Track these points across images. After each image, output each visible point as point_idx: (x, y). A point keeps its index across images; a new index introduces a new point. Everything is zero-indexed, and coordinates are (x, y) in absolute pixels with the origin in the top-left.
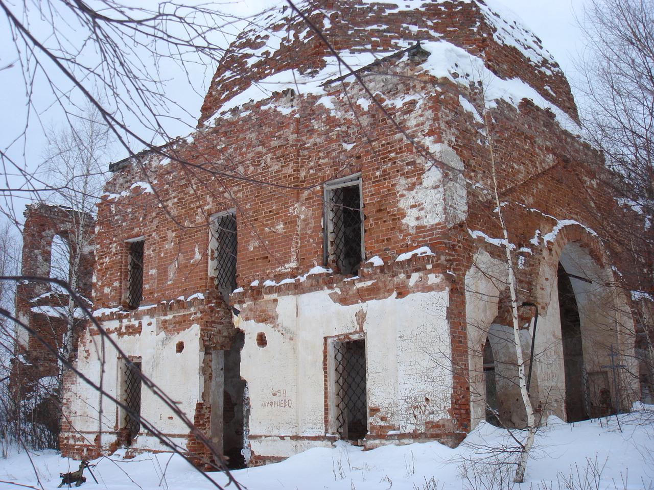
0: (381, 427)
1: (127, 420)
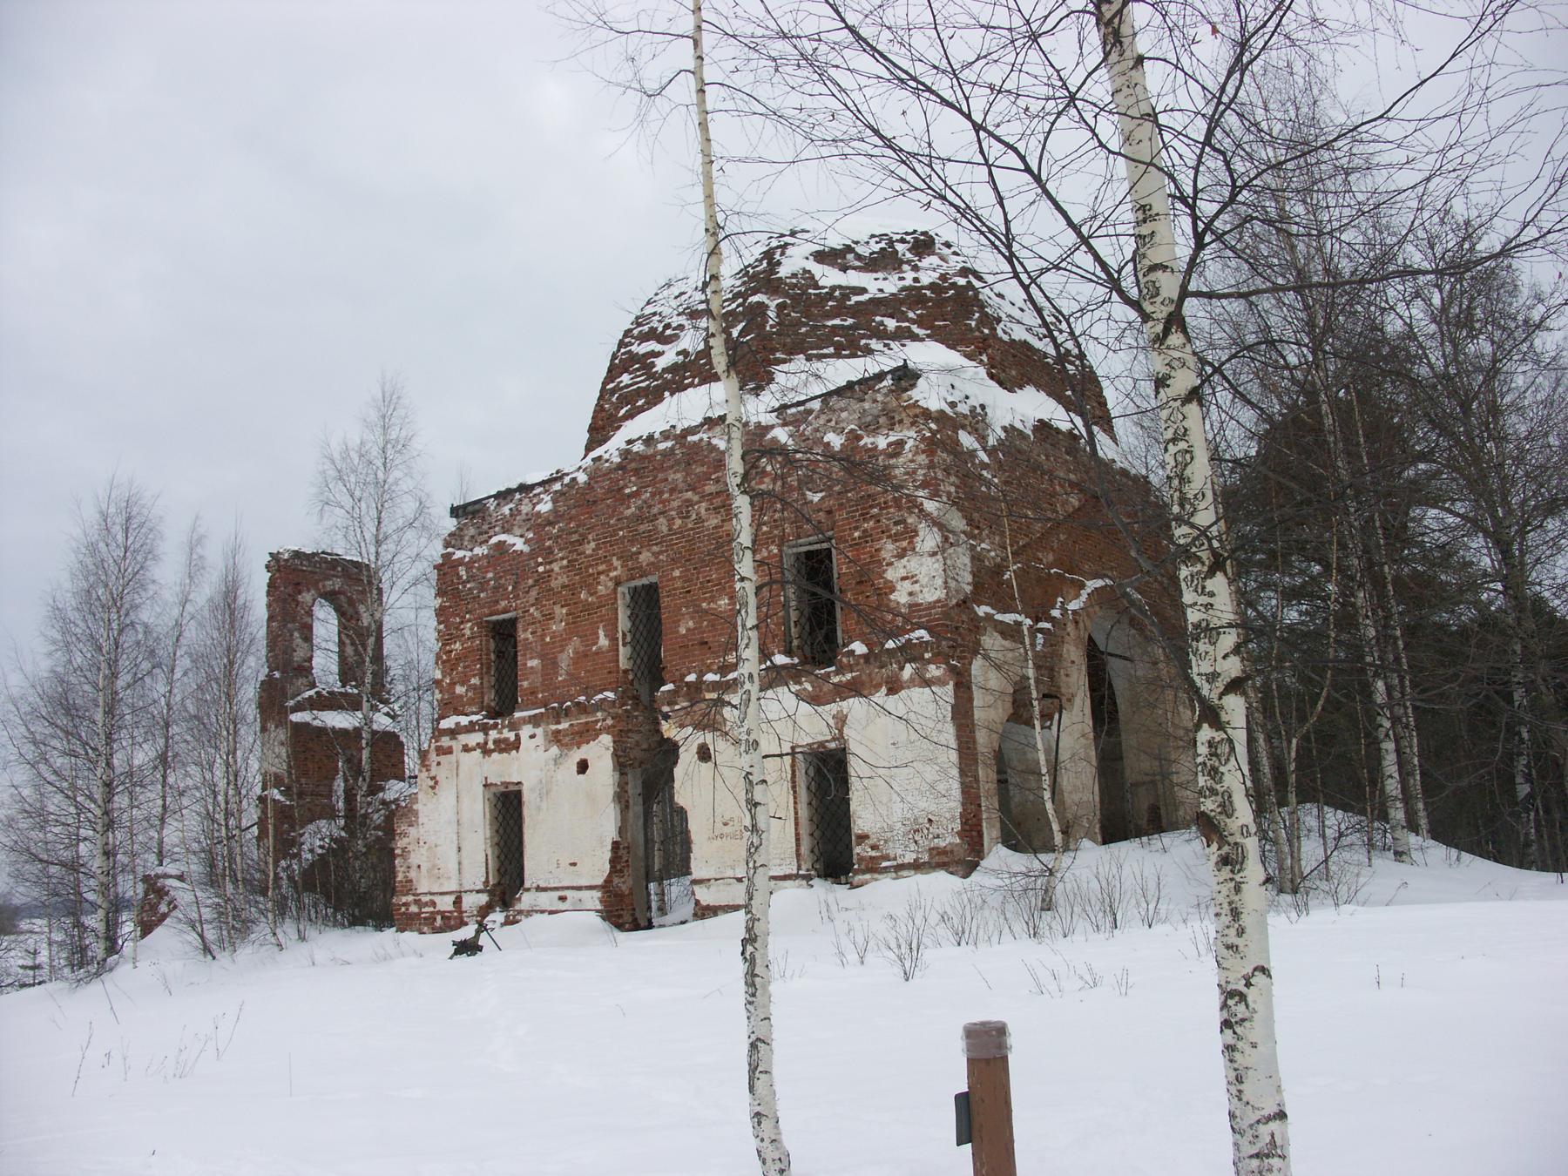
0: (871, 857)
1: (501, 871)
